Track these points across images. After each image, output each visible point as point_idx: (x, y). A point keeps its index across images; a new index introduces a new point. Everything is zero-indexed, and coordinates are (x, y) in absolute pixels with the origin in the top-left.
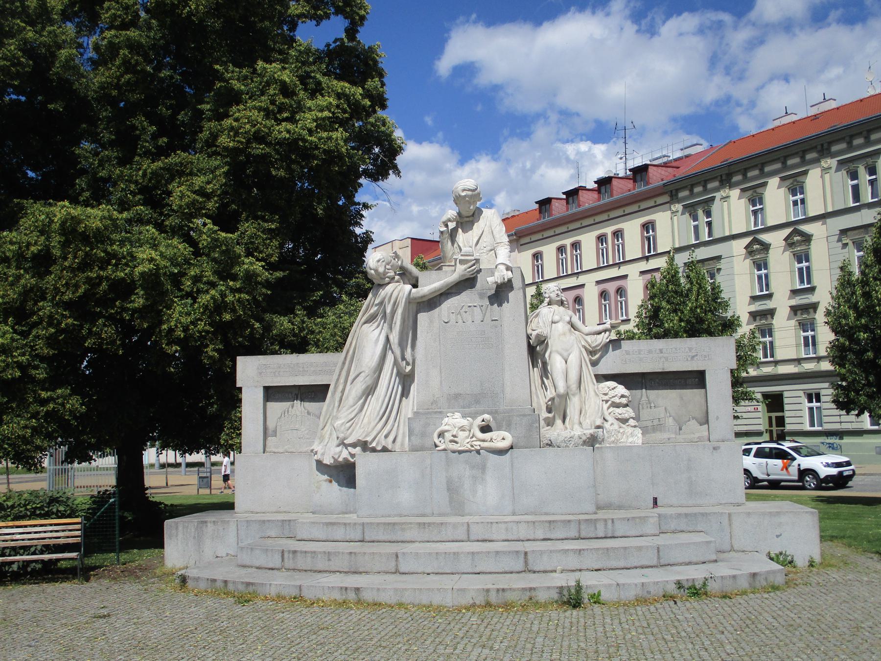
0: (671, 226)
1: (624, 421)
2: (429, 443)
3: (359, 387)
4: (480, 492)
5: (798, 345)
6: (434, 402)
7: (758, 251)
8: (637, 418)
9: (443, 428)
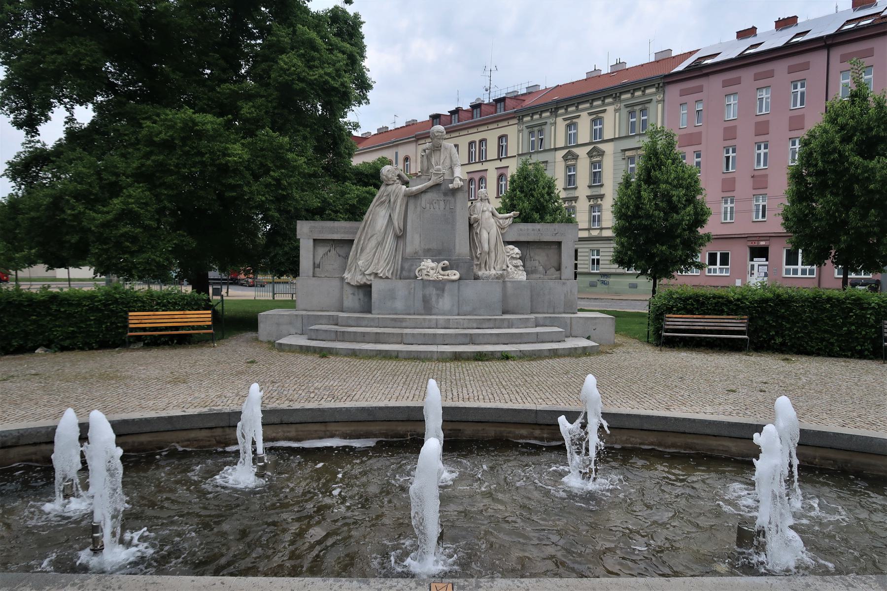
0: (516, 136)
1: (516, 267)
2: (412, 275)
3: (373, 243)
4: (441, 303)
5: (590, 221)
6: (416, 253)
7: (570, 157)
8: (524, 266)
9: (422, 267)
